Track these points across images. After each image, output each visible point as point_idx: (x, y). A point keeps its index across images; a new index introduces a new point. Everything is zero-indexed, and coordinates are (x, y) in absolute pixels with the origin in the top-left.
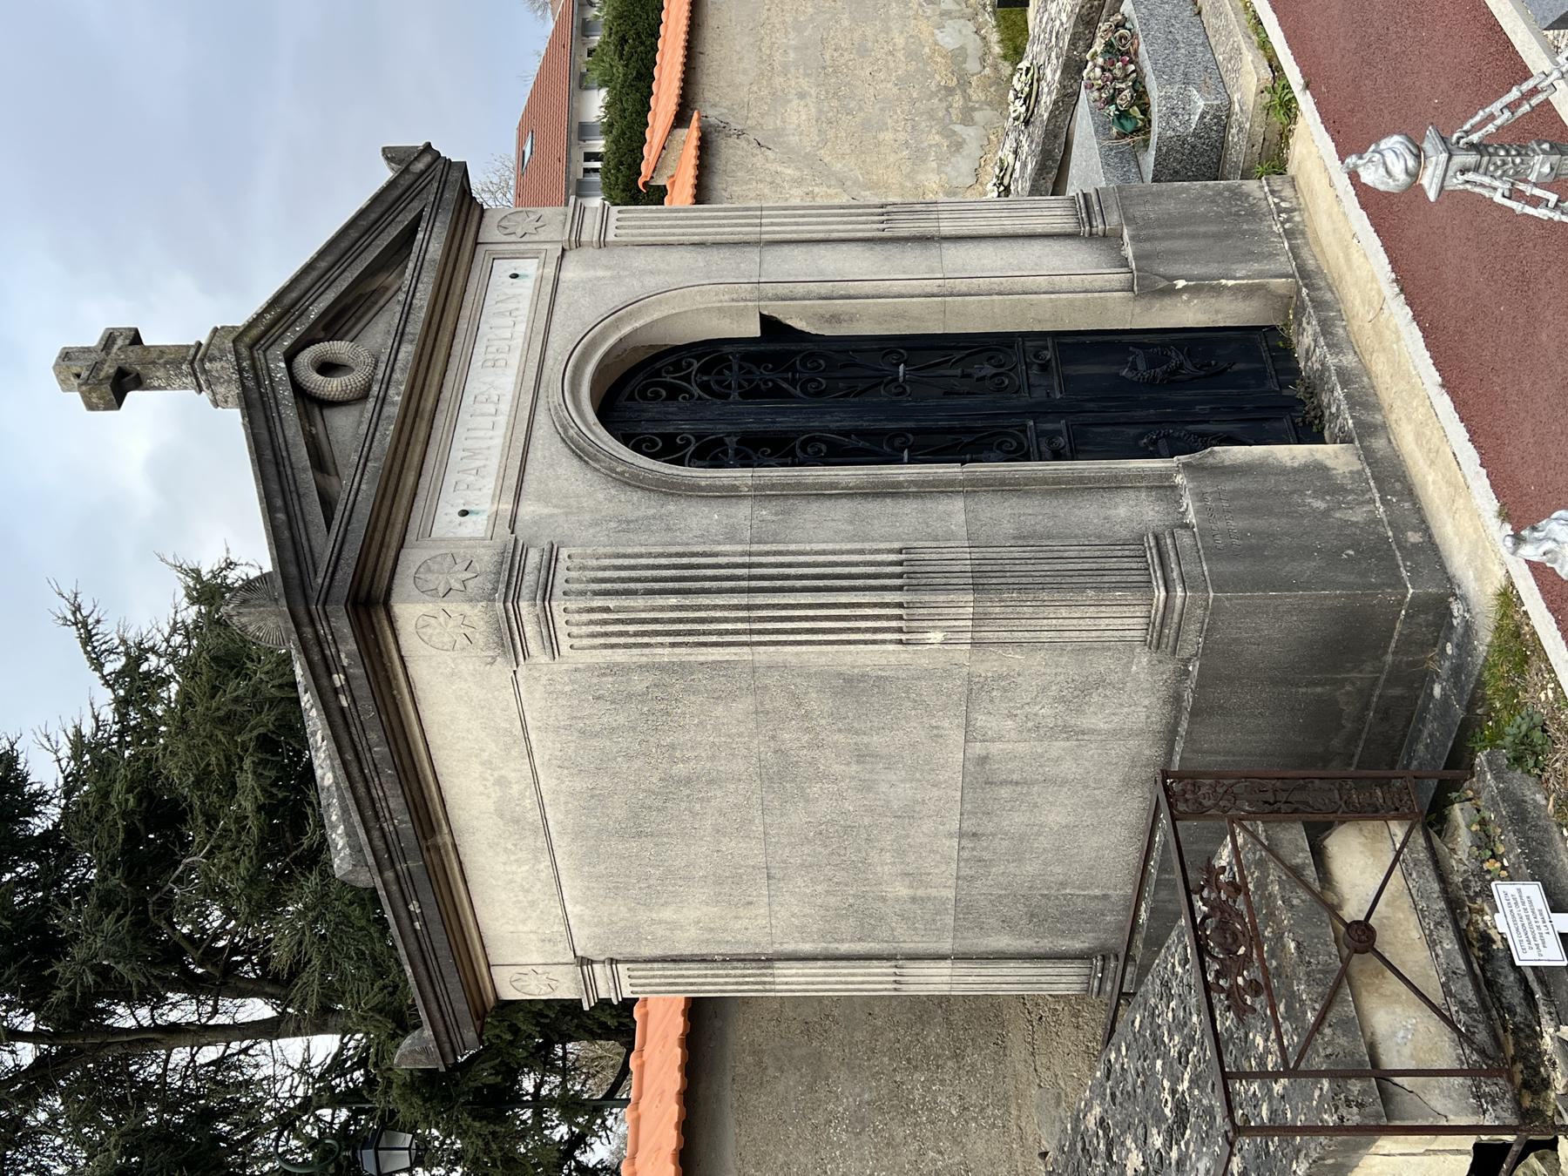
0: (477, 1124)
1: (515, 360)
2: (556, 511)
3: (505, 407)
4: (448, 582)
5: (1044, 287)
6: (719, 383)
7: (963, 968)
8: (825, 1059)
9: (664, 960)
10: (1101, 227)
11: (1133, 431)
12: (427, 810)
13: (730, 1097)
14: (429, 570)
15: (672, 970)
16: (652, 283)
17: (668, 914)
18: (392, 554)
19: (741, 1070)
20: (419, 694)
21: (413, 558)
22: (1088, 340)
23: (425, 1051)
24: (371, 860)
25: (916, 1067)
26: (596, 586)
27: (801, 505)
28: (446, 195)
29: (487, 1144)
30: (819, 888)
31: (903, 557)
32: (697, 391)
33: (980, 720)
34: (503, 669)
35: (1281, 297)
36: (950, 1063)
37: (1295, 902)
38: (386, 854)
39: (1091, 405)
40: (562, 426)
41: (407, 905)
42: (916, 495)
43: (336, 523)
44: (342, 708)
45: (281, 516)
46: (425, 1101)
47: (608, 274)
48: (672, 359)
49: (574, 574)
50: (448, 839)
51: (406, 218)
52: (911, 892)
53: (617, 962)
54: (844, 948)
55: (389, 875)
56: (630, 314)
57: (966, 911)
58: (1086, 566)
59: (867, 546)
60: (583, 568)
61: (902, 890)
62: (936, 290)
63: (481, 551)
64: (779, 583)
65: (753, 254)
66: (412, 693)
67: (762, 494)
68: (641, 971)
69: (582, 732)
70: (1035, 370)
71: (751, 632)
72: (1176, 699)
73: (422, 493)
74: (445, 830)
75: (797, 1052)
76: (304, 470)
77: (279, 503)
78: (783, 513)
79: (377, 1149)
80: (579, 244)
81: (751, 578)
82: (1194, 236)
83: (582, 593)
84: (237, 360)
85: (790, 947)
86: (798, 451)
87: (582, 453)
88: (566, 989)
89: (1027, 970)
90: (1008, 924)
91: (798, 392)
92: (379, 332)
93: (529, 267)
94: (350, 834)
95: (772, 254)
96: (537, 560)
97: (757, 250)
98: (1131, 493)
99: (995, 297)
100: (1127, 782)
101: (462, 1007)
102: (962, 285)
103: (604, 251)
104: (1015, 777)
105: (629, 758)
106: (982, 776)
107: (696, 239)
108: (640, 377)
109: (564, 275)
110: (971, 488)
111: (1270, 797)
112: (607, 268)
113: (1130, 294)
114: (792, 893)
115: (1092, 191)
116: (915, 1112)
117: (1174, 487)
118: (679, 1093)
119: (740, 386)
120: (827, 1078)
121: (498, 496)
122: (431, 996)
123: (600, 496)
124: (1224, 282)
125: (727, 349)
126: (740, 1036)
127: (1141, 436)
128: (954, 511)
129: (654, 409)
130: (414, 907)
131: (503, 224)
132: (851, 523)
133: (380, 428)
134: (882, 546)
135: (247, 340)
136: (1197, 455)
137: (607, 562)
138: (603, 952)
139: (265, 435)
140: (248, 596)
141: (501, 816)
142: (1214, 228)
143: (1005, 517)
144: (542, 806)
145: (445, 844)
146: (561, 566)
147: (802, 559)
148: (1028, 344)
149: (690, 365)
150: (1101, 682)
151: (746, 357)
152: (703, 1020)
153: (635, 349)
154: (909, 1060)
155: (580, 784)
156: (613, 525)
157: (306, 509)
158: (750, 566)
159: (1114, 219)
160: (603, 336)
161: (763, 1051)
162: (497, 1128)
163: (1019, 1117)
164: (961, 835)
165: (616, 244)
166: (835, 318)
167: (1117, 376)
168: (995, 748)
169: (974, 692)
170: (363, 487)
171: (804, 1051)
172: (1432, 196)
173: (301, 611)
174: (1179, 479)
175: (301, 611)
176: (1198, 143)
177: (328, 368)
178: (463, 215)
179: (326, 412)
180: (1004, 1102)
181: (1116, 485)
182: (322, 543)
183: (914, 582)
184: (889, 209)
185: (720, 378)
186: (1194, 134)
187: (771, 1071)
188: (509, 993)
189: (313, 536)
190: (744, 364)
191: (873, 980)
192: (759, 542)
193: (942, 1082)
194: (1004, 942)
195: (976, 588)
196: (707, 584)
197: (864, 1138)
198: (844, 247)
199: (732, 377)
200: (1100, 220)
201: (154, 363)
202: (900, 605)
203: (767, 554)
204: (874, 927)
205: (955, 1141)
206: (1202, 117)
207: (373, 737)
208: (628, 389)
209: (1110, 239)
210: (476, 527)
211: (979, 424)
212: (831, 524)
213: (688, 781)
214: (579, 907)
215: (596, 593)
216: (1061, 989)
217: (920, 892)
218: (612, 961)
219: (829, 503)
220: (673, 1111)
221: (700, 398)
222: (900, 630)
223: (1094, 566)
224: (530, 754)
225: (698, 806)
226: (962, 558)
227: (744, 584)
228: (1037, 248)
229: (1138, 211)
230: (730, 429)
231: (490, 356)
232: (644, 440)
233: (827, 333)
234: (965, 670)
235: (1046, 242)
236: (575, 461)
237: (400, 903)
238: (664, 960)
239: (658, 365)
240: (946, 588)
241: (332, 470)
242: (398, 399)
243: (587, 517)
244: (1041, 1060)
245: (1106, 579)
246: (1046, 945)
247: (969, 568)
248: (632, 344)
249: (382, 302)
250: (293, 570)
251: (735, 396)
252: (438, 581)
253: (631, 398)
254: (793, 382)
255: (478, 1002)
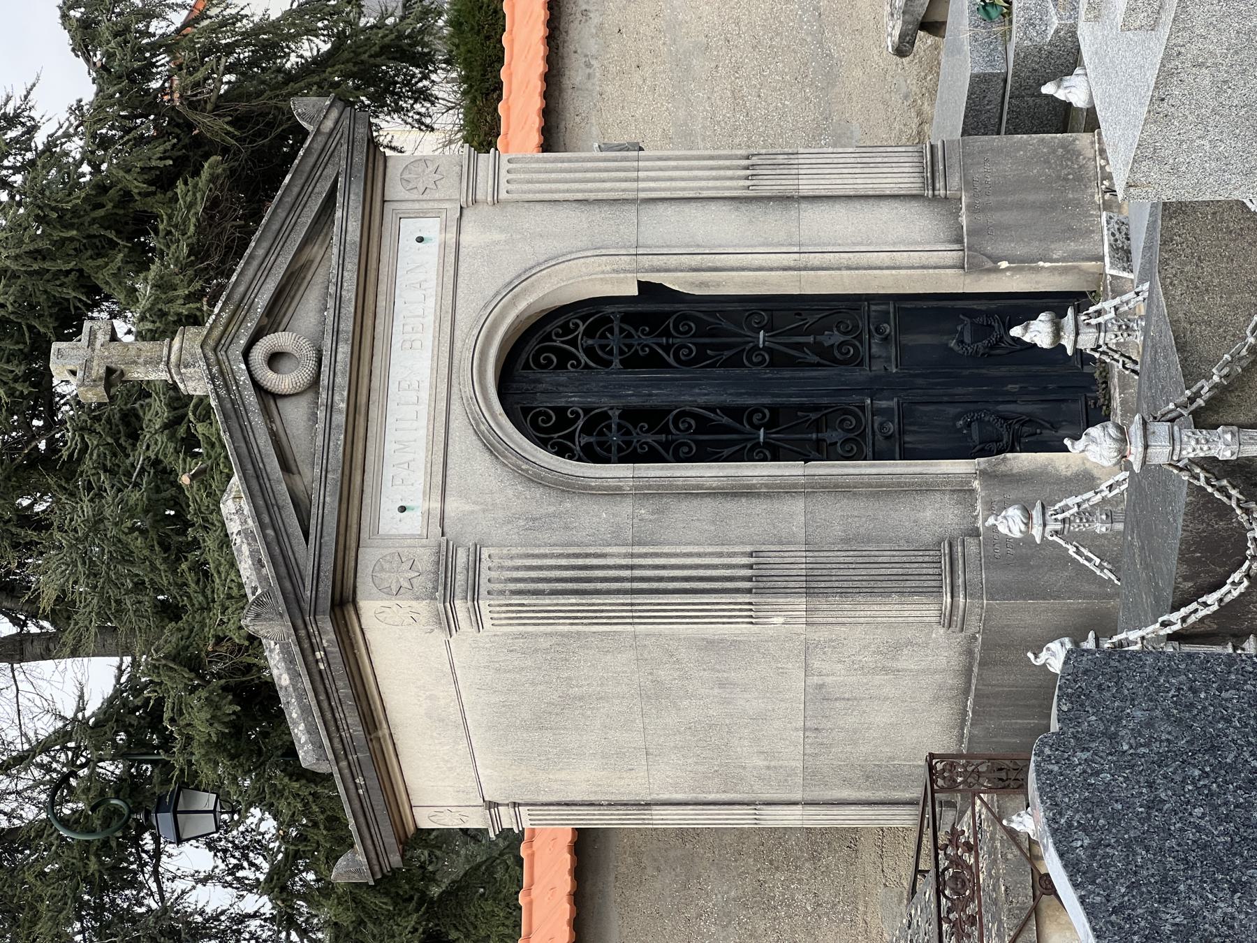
0: (296, 785)
1: (428, 339)
2: (477, 508)
3: (425, 395)
4: (398, 581)
5: (888, 263)
6: (603, 347)
7: (812, 810)
8: (697, 860)
9: (559, 804)
10: (942, 192)
11: (952, 410)
12: (371, 717)
13: (613, 894)
14: (382, 569)
15: (565, 811)
16: (544, 249)
17: (562, 775)
18: (353, 554)
19: (623, 869)
20: (372, 648)
21: (369, 558)
22: (924, 304)
23: (359, 871)
24: (331, 756)
25: (777, 868)
26: (512, 586)
27: (673, 503)
28: (356, 159)
29: (306, 805)
30: (690, 761)
31: (753, 560)
32: (584, 359)
33: (816, 664)
34: (441, 636)
35: (1093, 273)
36: (807, 865)
37: (1009, 856)
38: (342, 751)
39: (920, 381)
40: (474, 418)
41: (354, 779)
42: (768, 495)
43: (312, 537)
44: (320, 671)
45: (270, 532)
46: (232, 757)
47: (503, 237)
48: (561, 321)
49: (494, 574)
50: (386, 732)
51: (324, 188)
52: (766, 763)
53: (519, 805)
54: (711, 797)
55: (344, 764)
56: (525, 290)
57: (811, 775)
58: (895, 571)
59: (725, 549)
60: (501, 568)
61: (760, 762)
62: (792, 264)
63: (420, 551)
64: (655, 585)
65: (630, 213)
66: (367, 649)
67: (644, 493)
68: (538, 811)
69: (498, 670)
70: (876, 339)
71: (633, 617)
72: (970, 652)
73: (367, 490)
74: (385, 726)
75: (672, 854)
76: (279, 482)
77: (267, 520)
78: (658, 512)
79: (175, 813)
80: (475, 201)
81: (633, 579)
82: (1021, 206)
83: (502, 593)
84: (208, 365)
85: (665, 796)
86: (671, 426)
87: (493, 448)
88: (475, 820)
89: (868, 811)
90: (847, 782)
91: (671, 360)
92: (308, 312)
93: (430, 228)
94: (312, 730)
95: (649, 212)
96: (465, 560)
97: (634, 208)
98: (938, 495)
99: (845, 272)
100: (936, 699)
101: (391, 841)
102: (816, 260)
103: (498, 208)
104: (846, 696)
105: (533, 684)
106: (819, 696)
107: (580, 196)
108: (533, 342)
109: (465, 239)
110: (811, 489)
111: (1003, 775)
112: (502, 230)
113: (961, 271)
114: (667, 763)
115: (939, 144)
116: (775, 907)
117: (973, 491)
118: (570, 894)
119: (621, 352)
120: (699, 877)
121: (427, 494)
122: (367, 835)
123: (510, 493)
124: (1041, 264)
125: (609, 309)
126: (619, 865)
127: (958, 417)
128: (794, 516)
129: (548, 378)
130: (360, 781)
131: (406, 176)
132: (713, 522)
133: (332, 438)
134: (737, 549)
135: (211, 342)
136: (993, 459)
137: (519, 562)
138: (507, 798)
139: (244, 450)
140: (259, 610)
141: (430, 718)
142: (1041, 197)
143: (838, 517)
144: (463, 712)
145: (384, 736)
146: (485, 564)
147: (673, 561)
148: (873, 308)
149: (577, 326)
150: (909, 643)
151: (626, 318)
152: (587, 848)
153: (529, 317)
154: (771, 862)
155: (495, 699)
156: (521, 523)
157: (286, 520)
158: (632, 567)
159: (955, 181)
160: (502, 316)
161: (642, 853)
162: (319, 790)
163: (865, 913)
164: (805, 730)
165: (508, 202)
166: (703, 284)
167: (946, 347)
168: (829, 680)
169: (808, 649)
170: (327, 499)
171: (679, 853)
172: (1038, 541)
173: (300, 623)
174: (976, 484)
175: (300, 623)
176: (1055, 50)
177: (274, 359)
178: (370, 165)
179: (280, 403)
180: (853, 900)
181: (925, 488)
182: (304, 555)
183: (761, 585)
184: (755, 160)
185: (604, 342)
186: (1050, 44)
187: (649, 871)
188: (425, 824)
189: (296, 549)
190: (625, 326)
191: (740, 818)
192: (639, 544)
193: (800, 881)
194: (846, 794)
195: (809, 592)
196: (599, 586)
197: (731, 930)
198: (713, 206)
199: (614, 341)
200: (942, 180)
201: (135, 363)
202: (750, 604)
203: (645, 555)
204: (736, 784)
205: (809, 933)
206: (1057, 31)
207: (340, 684)
208: (522, 360)
209: (948, 203)
210: (412, 524)
211: (825, 401)
212: (698, 524)
213: (581, 698)
214: (488, 771)
215: (514, 593)
216: (896, 824)
217: (773, 764)
218: (515, 805)
219: (695, 502)
220: (564, 910)
221: (587, 366)
222: (751, 617)
223: (900, 571)
224: (456, 682)
225: (589, 712)
226: (797, 559)
227: (627, 585)
228: (885, 211)
229: (977, 173)
230: (613, 402)
231: (407, 337)
232: (540, 413)
233: (697, 293)
234: (803, 637)
235: (895, 204)
236: (487, 456)
237: (349, 780)
238: (559, 804)
239: (548, 329)
240: (786, 591)
241: (294, 469)
242: (343, 406)
243: (500, 514)
244: (888, 862)
245: (908, 584)
246: (881, 795)
247: (803, 572)
248: (531, 312)
249: (309, 277)
250: (288, 585)
251: (616, 363)
252: (391, 580)
253: (527, 366)
254: (667, 348)
255: (401, 832)
